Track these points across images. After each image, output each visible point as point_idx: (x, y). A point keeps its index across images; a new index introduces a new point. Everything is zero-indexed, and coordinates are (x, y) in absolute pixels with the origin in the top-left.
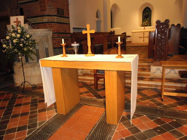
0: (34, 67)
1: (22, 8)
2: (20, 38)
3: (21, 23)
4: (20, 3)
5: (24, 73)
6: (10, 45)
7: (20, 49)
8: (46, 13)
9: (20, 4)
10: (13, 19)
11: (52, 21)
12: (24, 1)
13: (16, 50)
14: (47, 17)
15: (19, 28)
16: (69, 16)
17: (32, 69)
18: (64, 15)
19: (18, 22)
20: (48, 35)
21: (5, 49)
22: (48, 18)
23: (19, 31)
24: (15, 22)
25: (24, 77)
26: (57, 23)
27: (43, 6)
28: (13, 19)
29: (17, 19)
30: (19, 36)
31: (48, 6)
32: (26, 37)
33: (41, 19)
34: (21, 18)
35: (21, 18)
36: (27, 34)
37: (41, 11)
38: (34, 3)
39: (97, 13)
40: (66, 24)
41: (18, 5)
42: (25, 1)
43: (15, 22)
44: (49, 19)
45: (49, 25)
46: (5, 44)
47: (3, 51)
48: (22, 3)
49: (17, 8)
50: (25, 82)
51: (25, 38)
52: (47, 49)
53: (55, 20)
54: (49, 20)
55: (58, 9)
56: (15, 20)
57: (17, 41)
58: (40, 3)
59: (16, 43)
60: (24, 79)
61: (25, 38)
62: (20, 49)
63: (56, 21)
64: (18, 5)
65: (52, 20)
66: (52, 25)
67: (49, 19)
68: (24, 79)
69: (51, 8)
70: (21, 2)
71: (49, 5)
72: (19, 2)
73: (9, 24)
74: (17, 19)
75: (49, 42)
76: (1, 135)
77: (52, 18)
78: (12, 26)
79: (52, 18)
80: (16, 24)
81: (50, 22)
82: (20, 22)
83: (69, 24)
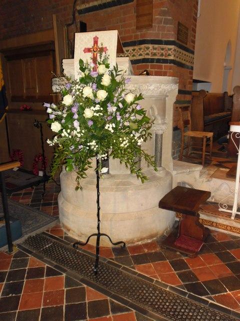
0: (125, 190)
1: (85, 24)
2: (104, 104)
3: (108, 53)
4: (81, 10)
5: (99, 209)
6: (76, 124)
7: (104, 139)
8: (151, 34)
9: (80, 12)
10: (83, 40)
11: (164, 58)
12: (91, 4)
13: (94, 143)
14: (151, 46)
15: (102, 69)
16: (194, 47)
17: (119, 195)
18: (187, 44)
19: (97, 50)
20: (167, 96)
21: (53, 135)
22: (154, 49)
23: (106, 81)
24: (88, 50)
25: (99, 220)
26: (174, 64)
27: (145, 15)
28: (83, 40)
29: (96, 41)
30: (102, 95)
31: (159, 14)
32: (124, 102)
33: (134, 50)
34: (109, 39)
35: (109, 39)
36: (95, 96)
37: (139, 28)
38: (119, 6)
39: (228, 44)
40: (188, 67)
41: (74, 15)
42: (96, 3)
43: (88, 50)
44: (155, 51)
45: (152, 67)
46: (58, 119)
47: (49, 142)
48: (89, 8)
49: (73, 23)
50: (99, 235)
51: (121, 105)
52: (160, 137)
53: (169, 55)
54: (155, 54)
55: (179, 24)
56: (90, 45)
57: (97, 111)
58: (138, 5)
59: (93, 119)
60: (98, 228)
61: (121, 105)
62: (104, 139)
63: (172, 58)
64: (74, 15)
65: (162, 55)
66: (161, 67)
67: (155, 51)
68: (98, 228)
69: (166, 22)
70: (83, 7)
71: (165, 10)
72: (78, 8)
73: (71, 55)
74: (96, 41)
75: (166, 117)
76: (3, 269)
77: (163, 49)
78: (81, 62)
79: (163, 49)
80: (90, 55)
81: (158, 61)
82: (102, 50)
83: (192, 68)
